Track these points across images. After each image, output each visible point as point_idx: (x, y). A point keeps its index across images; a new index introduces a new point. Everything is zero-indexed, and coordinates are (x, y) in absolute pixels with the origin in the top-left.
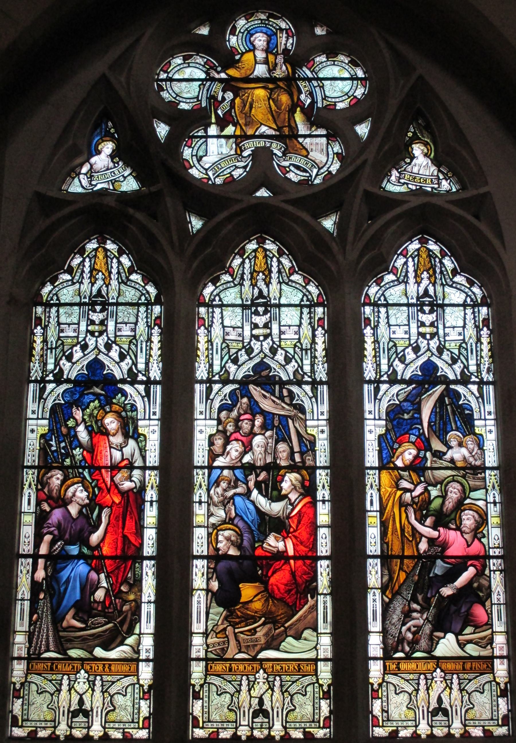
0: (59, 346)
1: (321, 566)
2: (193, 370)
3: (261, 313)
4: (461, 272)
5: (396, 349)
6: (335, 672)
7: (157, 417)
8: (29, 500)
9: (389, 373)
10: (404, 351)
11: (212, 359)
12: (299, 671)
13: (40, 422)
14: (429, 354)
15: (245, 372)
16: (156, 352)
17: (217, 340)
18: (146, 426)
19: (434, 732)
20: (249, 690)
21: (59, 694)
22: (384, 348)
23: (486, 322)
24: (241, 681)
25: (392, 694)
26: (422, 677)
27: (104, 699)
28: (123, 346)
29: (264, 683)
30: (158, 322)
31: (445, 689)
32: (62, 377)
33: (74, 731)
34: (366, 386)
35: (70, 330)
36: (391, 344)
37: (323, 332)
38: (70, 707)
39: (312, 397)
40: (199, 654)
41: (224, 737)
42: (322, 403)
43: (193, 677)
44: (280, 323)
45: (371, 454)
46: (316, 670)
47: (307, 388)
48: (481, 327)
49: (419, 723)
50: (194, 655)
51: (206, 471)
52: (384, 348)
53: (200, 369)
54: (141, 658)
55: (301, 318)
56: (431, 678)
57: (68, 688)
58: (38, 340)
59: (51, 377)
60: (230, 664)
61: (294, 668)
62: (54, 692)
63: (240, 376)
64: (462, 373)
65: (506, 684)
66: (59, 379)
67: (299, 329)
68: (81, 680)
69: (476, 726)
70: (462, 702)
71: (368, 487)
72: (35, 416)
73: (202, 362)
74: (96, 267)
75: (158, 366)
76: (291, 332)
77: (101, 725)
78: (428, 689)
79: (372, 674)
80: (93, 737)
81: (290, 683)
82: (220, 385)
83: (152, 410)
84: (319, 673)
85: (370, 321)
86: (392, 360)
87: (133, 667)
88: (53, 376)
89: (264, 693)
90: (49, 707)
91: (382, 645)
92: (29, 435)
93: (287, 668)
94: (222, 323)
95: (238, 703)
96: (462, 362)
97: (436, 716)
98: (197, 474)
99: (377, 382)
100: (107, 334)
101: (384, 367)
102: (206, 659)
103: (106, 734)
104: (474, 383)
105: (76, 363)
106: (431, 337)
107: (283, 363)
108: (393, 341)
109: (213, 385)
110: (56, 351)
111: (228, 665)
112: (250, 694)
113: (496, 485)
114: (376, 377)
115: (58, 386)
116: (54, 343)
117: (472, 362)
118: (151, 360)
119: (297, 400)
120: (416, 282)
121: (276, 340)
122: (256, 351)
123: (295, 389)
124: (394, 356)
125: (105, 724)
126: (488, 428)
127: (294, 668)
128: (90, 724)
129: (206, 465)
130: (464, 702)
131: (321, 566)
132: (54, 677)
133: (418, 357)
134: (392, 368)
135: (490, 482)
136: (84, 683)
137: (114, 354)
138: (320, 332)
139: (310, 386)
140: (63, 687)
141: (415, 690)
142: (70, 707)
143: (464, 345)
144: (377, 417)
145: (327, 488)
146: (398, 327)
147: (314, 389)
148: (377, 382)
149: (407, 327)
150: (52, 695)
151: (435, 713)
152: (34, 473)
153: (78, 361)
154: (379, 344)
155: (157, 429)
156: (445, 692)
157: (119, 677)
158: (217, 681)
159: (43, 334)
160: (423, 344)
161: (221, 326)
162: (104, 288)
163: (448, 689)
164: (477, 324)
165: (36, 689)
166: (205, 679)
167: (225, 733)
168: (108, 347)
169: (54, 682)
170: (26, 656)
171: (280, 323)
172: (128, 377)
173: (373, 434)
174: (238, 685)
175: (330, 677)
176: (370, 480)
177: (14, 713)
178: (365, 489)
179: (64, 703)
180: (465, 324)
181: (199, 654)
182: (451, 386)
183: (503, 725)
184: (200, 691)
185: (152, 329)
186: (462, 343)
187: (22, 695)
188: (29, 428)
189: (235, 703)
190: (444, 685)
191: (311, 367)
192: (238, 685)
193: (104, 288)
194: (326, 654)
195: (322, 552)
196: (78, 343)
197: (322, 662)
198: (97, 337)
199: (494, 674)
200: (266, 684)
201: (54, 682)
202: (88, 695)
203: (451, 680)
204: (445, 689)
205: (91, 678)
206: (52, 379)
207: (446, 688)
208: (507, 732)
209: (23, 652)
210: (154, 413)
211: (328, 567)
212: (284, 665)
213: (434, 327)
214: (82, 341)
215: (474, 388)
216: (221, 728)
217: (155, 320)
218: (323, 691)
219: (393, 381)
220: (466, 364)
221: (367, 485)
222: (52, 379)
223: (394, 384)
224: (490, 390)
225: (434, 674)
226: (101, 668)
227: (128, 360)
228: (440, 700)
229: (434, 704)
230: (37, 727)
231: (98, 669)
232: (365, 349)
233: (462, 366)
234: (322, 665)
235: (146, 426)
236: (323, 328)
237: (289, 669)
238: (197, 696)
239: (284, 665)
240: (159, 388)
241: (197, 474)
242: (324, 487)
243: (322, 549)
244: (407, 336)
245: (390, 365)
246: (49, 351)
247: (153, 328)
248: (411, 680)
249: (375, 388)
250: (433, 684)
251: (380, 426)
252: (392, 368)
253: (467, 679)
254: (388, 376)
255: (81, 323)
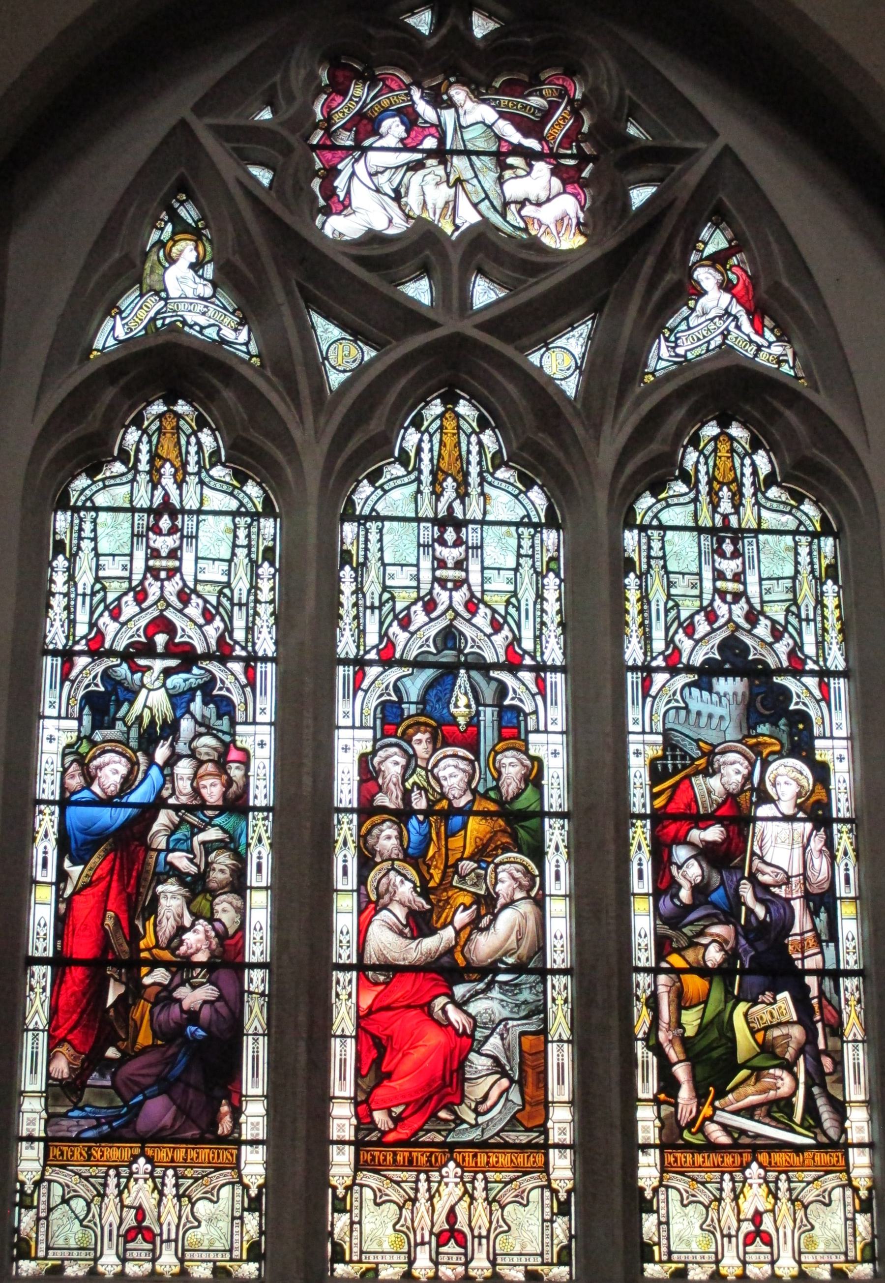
0: (98, 592)
1: (553, 987)
2: (333, 643)
3: (728, 555)
4: (783, 481)
5: (679, 613)
6: (273, 1164)
7: (266, 718)
8: (640, 872)
9: (381, 647)
10: (408, 608)
11: (651, 628)
12: (89, 1160)
13: (649, 738)
14: (161, 605)
15: (132, 636)
16: (552, 617)
17: (241, 585)
18: (828, 749)
19: (748, 1273)
20: (120, 1194)
21: (413, 1205)
22: (658, 611)
23: (831, 572)
24: (721, 1183)
25: (368, 1205)
26: (112, 1172)
27: (491, 1214)
28: (209, 598)
29: (456, 1184)
30: (553, 565)
31: (461, 1199)
32: (102, 645)
33: (442, 1268)
34: (341, 670)
35: (501, 579)
36: (386, 596)
37: (557, 581)
38: (433, 1225)
39: (246, 686)
40: (32, 1127)
41: (697, 1278)
42: (264, 692)
43: (332, 1172)
44: (482, 562)
45: (638, 792)
46: (547, 1163)
47: (812, 682)
48: (260, 562)
49: (723, 1256)
50: (335, 1134)
51: (56, 809)
52: (658, 611)
53: (344, 640)
54: (243, 1137)
55: (797, 563)
56: (438, 1179)
57: (732, 1195)
58: (60, 578)
59: (660, 662)
60: (410, 1153)
61: (81, 1154)
62: (711, 1202)
63: (698, 660)
64: (221, 640)
65: (260, 1188)
66: (96, 650)
67: (230, 566)
68: (451, 1179)
69: (515, 1265)
70: (180, 1218)
71: (634, 848)
72: (349, 723)
73: (348, 627)
74: (442, 465)
75: (270, 633)
76: (404, 575)
77: (488, 1258)
78: (431, 1198)
79: (641, 1172)
80: (162, 1274)
81: (191, 1181)
82: (667, 676)
83: (258, 706)
84: (551, 1170)
85: (351, 556)
86: (96, 616)
87: (540, 1159)
88: (87, 644)
89: (456, 1204)
90: (196, 1224)
91: (354, 1121)
92: (46, 746)
93: (382, 1158)
94: (381, 559)
95: (413, 1221)
96: (791, 636)
97: (133, 1240)
98: (339, 822)
99: (647, 670)
100: (182, 575)
101: (659, 645)
102: (239, 1143)
103: (802, 1274)
104: (239, 659)
105: (416, 632)
106: (455, 585)
107: (770, 639)
108: (673, 600)
109: (367, 669)
110: (91, 600)
111: (407, 1154)
112: (121, 1201)
113: (562, 845)
114: (66, 645)
115: (672, 677)
116: (376, 596)
117: (239, 623)
118: (827, 637)
119: (797, 703)
120: (433, 492)
121: (756, 602)
122: (721, 621)
123: (505, 677)
124: (391, 617)
125: (183, 1254)
126: (837, 753)
127: (81, 1154)
128: (775, 1257)
129: (57, 798)
130: (798, 1221)
131: (553, 987)
132: (94, 1171)
133: (713, 631)
134: (385, 640)
135: (254, 831)
136: (146, 1180)
137: (194, 610)
138: (266, 570)
139: (817, 679)
140: (108, 1191)
141: (99, 1194)
142: (433, 1225)
143: (794, 609)
144: (647, 729)
145: (564, 850)
146: (111, 558)
147: (249, 672)
148: (360, 663)
149: (128, 558)
150: (707, 1208)
151: (442, 1238)
152: (351, 821)
153: (130, 620)
154: (649, 603)
155: (562, 750)
156: (462, 1202)
157: (512, 1175)
158: (680, 1183)
159: (640, 586)
160: (442, 597)
161: (379, 564)
162: (457, 505)
163: (467, 1198)
164: (817, 574)
165: (61, 1193)
166: (355, 1178)
167: (76, 1268)
168: (184, 597)
169: (92, 1180)
170: (657, 1142)
171: (482, 562)
172: (218, 650)
173: (350, 752)
174: (101, 1184)
175: (263, 1171)
176: (636, 836)
177: (23, 1235)
178: (629, 851)
179: (111, 1218)
180: (797, 572)
181: (32, 1127)
182: (775, 679)
183: (560, 1263)
184: (652, 1198)
185: (544, 577)
186: (790, 606)
187: (35, 1203)
188: (632, 748)
189: (406, 1220)
190: (459, 1190)
191: (247, 634)
192: (101, 1184)
193: (457, 505)
194: (562, 1137)
195: (848, 963)
196: (419, 599)
197: (557, 1151)
198: (451, 590)
199: (548, 1175)
200: (460, 1186)
201: (92, 1180)
202: (464, 1204)
203: (163, 1177)
204: (461, 1199)
205: (468, 1176)
206: (663, 664)
207: (463, 1195)
208: (257, 1273)
209: (37, 1127)
210: (554, 722)
211: (858, 988)
212: (376, 1154)
213: (461, 569)
214: (137, 586)
215: (237, 667)
216: (68, 1259)
217: (548, 563)
218: (249, 1196)
219: (387, 660)
220: (798, 640)
221: (337, 842)
222: (663, 664)
223: (391, 667)
224: (268, 672)
225: (134, 1166)
226: (390, 1158)
227: (218, 622)
228: (452, 1215)
229: (441, 1224)
230: (686, 1263)
231: (72, 1156)
232: (627, 612)
233: (510, 636)
234: (557, 1156)
235: (828, 749)
236: (557, 575)
237: (385, 1160)
238: (340, 1207)
239: (65, 1149)
240: (270, 668)
241: (339, 822)
242: (557, 848)
243: (556, 956)
244: (696, 592)
245: (92, 625)
246: (80, 599)
247: (546, 576)
248: (92, 1177)
249: (355, 673)
250: (745, 1190)
251: (655, 744)
252: (385, 640)
253: (500, 1182)
254: (379, 652)
255: (135, 552)
